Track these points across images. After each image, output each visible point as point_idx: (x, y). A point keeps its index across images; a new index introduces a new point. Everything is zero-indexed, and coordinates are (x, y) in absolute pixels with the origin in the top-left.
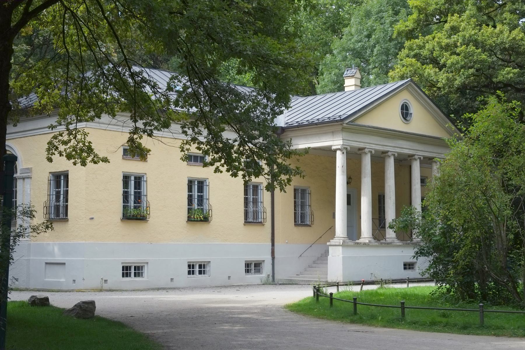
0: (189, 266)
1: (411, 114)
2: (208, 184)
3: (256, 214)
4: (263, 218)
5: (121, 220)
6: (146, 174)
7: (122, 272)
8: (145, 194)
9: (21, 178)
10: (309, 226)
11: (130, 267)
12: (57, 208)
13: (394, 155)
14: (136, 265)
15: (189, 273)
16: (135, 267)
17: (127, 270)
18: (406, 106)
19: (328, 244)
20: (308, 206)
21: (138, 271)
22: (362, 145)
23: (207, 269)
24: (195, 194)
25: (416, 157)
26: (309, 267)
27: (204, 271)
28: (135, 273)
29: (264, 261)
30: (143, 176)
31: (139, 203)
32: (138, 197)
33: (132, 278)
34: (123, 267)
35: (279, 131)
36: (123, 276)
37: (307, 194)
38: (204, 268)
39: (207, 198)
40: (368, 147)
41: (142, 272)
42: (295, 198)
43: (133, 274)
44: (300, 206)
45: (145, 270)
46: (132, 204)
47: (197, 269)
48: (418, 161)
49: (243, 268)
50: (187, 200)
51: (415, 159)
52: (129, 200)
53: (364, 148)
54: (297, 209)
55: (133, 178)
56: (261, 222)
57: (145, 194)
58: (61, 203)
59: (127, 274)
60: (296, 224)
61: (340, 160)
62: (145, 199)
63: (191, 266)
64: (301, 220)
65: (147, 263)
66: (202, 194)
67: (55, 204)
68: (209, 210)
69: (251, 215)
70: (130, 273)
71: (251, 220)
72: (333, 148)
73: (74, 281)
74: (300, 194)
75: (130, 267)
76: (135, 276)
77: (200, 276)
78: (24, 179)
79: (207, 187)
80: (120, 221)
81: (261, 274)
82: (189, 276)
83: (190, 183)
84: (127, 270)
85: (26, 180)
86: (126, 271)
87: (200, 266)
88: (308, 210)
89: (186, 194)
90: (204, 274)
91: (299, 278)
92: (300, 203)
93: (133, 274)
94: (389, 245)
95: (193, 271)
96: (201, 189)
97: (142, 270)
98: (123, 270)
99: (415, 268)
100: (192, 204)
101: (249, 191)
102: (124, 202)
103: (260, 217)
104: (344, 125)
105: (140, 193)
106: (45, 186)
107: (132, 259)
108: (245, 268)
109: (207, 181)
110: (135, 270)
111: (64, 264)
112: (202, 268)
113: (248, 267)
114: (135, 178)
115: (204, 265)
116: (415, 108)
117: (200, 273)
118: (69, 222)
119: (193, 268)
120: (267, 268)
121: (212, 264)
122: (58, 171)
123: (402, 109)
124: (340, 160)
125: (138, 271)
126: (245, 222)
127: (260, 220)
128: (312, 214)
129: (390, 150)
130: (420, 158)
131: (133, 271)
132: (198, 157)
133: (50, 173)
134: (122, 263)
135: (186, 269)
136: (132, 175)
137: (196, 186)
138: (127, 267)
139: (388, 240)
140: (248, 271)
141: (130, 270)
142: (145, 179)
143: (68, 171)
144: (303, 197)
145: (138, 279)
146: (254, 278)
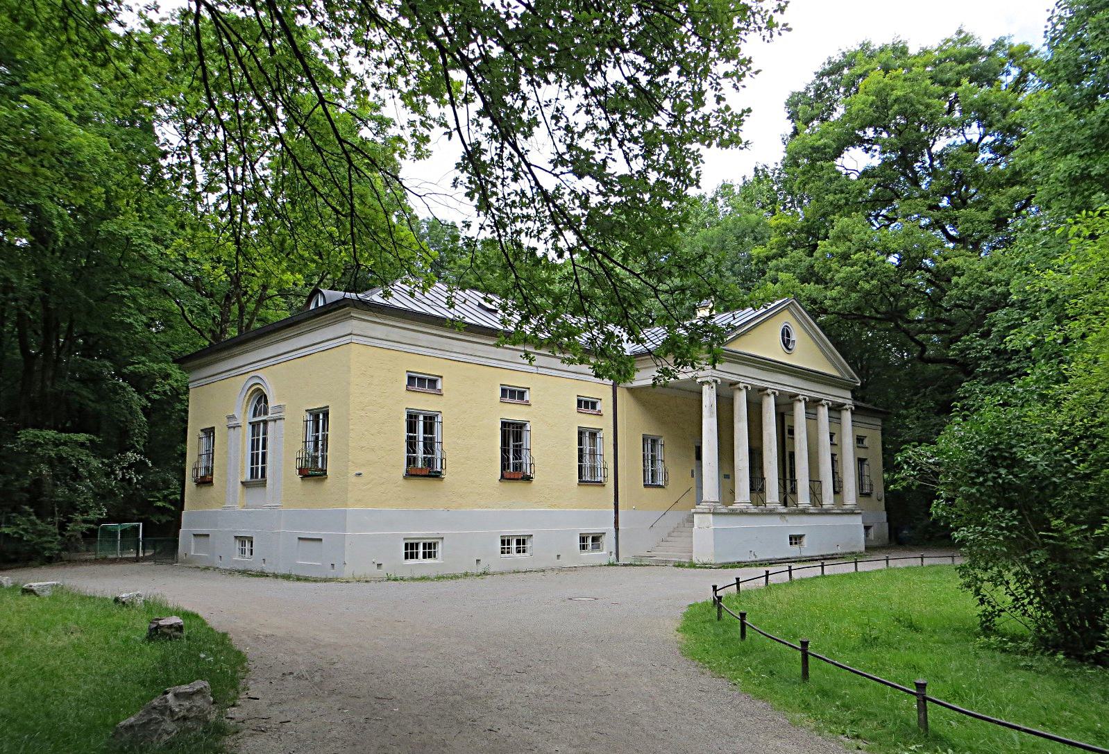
0: (503, 542)
11: (417, 544)
14: (412, 541)
16: (424, 545)
17: (412, 548)
19: (693, 510)
21: (430, 550)
22: (735, 378)
23: (528, 545)
24: (420, 434)
28: (424, 554)
32: (429, 446)
34: (406, 545)
36: (406, 558)
38: (524, 544)
43: (421, 555)
45: (439, 548)
46: (420, 454)
47: (514, 545)
55: (421, 418)
61: (709, 398)
70: (417, 553)
76: (424, 557)
78: (275, 420)
84: (412, 548)
86: (411, 550)
87: (518, 542)
88: (660, 467)
93: (421, 555)
96: (429, 428)
98: (406, 549)
102: (408, 452)
105: (432, 439)
106: (300, 430)
107: (420, 533)
110: (424, 548)
114: (425, 418)
115: (524, 540)
119: (508, 544)
120: (608, 542)
124: (709, 398)
125: (430, 550)
132: (514, 391)
138: (412, 545)
140: (583, 547)
145: (428, 561)
146: (590, 556)
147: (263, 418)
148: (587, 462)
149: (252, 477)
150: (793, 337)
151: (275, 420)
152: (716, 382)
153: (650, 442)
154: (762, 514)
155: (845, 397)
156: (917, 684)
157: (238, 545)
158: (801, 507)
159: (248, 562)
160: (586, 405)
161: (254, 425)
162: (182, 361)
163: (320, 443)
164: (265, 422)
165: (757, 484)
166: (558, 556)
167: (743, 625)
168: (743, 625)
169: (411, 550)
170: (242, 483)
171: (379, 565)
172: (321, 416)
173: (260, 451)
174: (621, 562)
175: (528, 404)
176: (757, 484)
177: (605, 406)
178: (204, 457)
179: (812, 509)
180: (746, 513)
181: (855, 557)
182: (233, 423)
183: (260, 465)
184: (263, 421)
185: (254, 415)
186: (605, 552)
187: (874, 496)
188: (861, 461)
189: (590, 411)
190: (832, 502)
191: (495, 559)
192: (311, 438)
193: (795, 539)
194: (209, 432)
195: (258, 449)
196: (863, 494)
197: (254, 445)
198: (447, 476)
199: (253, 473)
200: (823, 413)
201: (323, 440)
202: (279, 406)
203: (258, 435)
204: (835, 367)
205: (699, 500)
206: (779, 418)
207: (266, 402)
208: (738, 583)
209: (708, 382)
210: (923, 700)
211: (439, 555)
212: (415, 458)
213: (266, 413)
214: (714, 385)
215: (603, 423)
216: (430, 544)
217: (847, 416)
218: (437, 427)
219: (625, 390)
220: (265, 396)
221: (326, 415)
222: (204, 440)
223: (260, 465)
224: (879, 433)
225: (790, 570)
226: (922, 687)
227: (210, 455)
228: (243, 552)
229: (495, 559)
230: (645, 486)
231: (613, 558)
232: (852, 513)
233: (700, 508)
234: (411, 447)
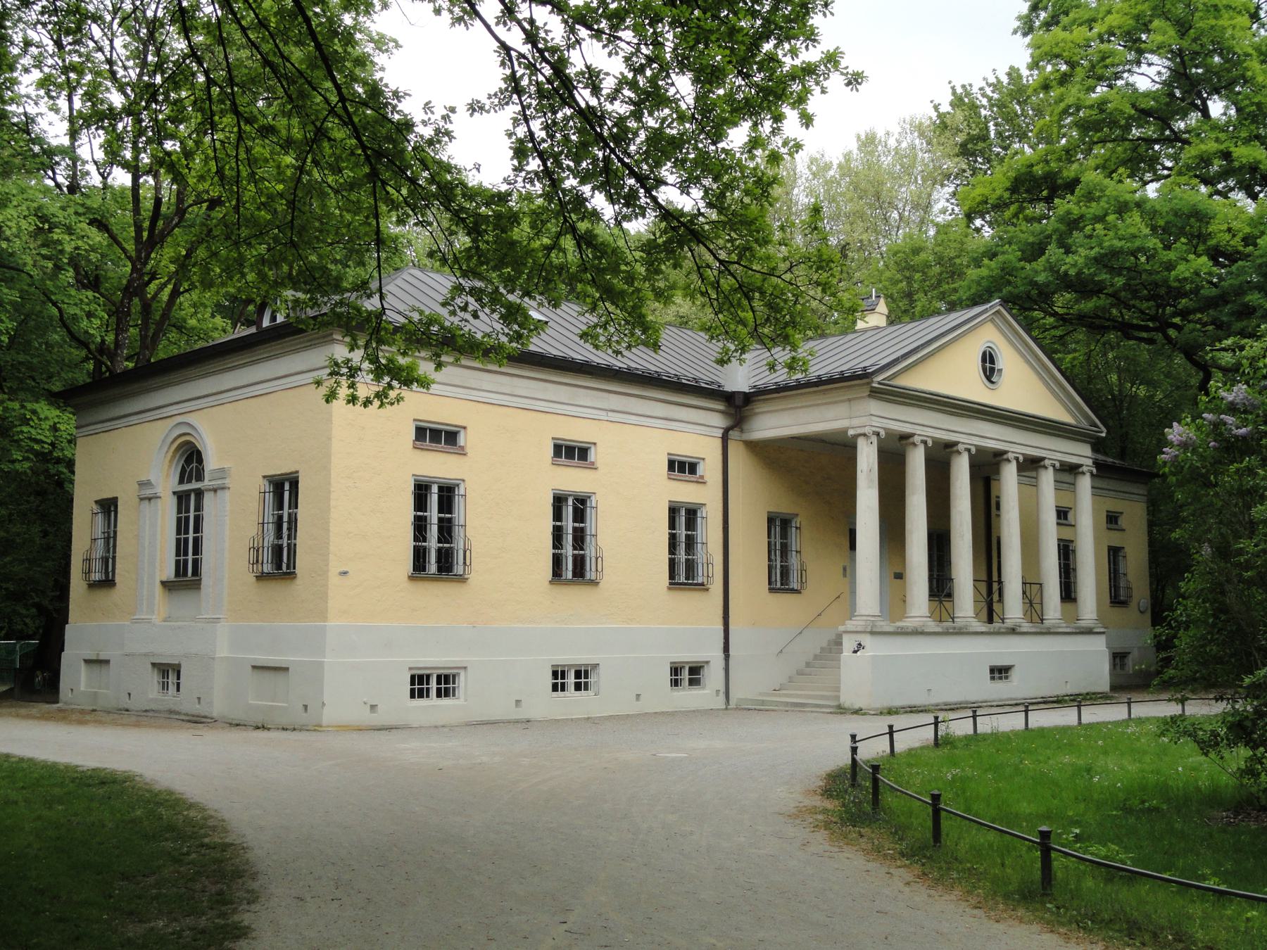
0: (555, 674)
1: (1000, 371)
2: (594, 505)
3: (691, 567)
4: (705, 574)
5: (409, 577)
6: (463, 481)
7: (409, 687)
8: (462, 522)
9: (210, 490)
10: (797, 592)
11: (428, 676)
12: (277, 550)
13: (969, 450)
15: (555, 688)
16: (439, 677)
17: (421, 683)
18: (991, 355)
19: (841, 628)
20: (794, 553)
21: (446, 684)
22: (907, 429)
24: (433, 514)
25: (1010, 456)
26: (800, 673)
27: (586, 684)
28: (439, 690)
29: (707, 662)
30: (458, 485)
31: (582, 549)
33: (433, 701)
34: (413, 677)
35: (739, 401)
36: (412, 696)
37: (794, 529)
38: (586, 677)
39: (593, 533)
40: (918, 432)
41: (454, 689)
42: (769, 536)
43: (433, 692)
44: (778, 553)
45: (461, 681)
47: (571, 680)
48: (1014, 464)
49: (667, 676)
50: (551, 537)
51: (1008, 460)
52: (564, 543)
53: (912, 435)
54: (773, 557)
55: (435, 489)
56: (702, 584)
57: (462, 522)
58: (285, 542)
59: (421, 691)
60: (772, 590)
61: (867, 460)
62: (462, 535)
63: (558, 674)
64: (782, 579)
65: (465, 668)
66: (582, 525)
67: (276, 542)
68: (597, 559)
69: (682, 570)
70: (428, 689)
71: (683, 579)
72: (851, 432)
73: (306, 707)
74: (778, 529)
75: (428, 676)
76: (439, 695)
77: (578, 693)
78: (215, 490)
79: (593, 511)
80: (406, 578)
81: (704, 688)
82: (555, 694)
83: (559, 501)
84: (421, 683)
85: (219, 492)
86: (419, 685)
87: (578, 674)
88: (794, 561)
89: (548, 524)
90: (586, 689)
91: (780, 696)
92: (778, 547)
94: (961, 632)
95: (563, 685)
96: (579, 515)
97: (454, 683)
98: (412, 683)
99: (1010, 679)
100: (451, 537)
101: (677, 519)
103: (700, 573)
104: (874, 385)
107: (433, 659)
108: (669, 678)
109: (593, 498)
110: (439, 682)
111: (287, 669)
112: (583, 677)
113: (676, 674)
114: (441, 489)
115: (586, 672)
116: (1010, 361)
117: (578, 687)
118: (299, 581)
119: (563, 678)
120: (713, 676)
121: (602, 669)
122: (279, 473)
123: (984, 360)
124: (867, 460)
125: (446, 684)
126: (670, 584)
127: (700, 581)
128: (803, 570)
129: (962, 440)
130: (1017, 459)
131: (433, 685)
132: (574, 448)
133: (264, 477)
134: (410, 669)
135: (549, 681)
136: (434, 483)
137: (570, 509)
138: (421, 677)
139: (959, 622)
140: (675, 683)
141: (428, 684)
142: (462, 492)
143: (297, 472)
144: (784, 535)
145: (444, 702)
146: (688, 697)
147: (194, 485)
148: (682, 556)
149: (177, 574)
150: (1000, 364)
151: (215, 490)
152: (878, 434)
153: (779, 525)
154: (946, 633)
155: (1081, 454)
156: (1041, 832)
157: (155, 677)
158: (1009, 623)
159: (170, 699)
160: (682, 467)
161: (182, 498)
162: (69, 398)
163: (285, 526)
164: (199, 494)
165: (941, 586)
166: (638, 696)
167: (937, 812)
168: (937, 812)
169: (419, 685)
170: (163, 583)
171: (373, 707)
172: (287, 487)
173: (191, 535)
174: (733, 704)
175: (592, 467)
176: (941, 586)
177: (710, 469)
178: (101, 543)
179: (1026, 627)
180: (923, 633)
181: (1079, 700)
182: (148, 492)
183: (190, 557)
184: (194, 490)
185: (181, 481)
186: (706, 695)
187: (1133, 604)
188: (1115, 553)
189: (687, 476)
190: (1058, 615)
191: (545, 703)
192: (270, 518)
193: (1000, 672)
194: (108, 507)
195: (187, 532)
196: (1117, 596)
197: (181, 526)
198: (473, 577)
199: (180, 569)
200: (1047, 479)
201: (289, 522)
202: (222, 470)
203: (188, 511)
204: (1069, 410)
205: (852, 611)
206: (981, 485)
207: (200, 461)
208: (891, 732)
209: (864, 435)
210: (1046, 850)
211: (461, 692)
212: (425, 548)
213: (200, 477)
214: (874, 438)
215: (706, 495)
216: (447, 677)
217: (1085, 484)
218: (458, 502)
219: (741, 447)
220: (199, 453)
221: (294, 483)
222: (100, 517)
223: (190, 557)
224: (1144, 506)
225: (936, 723)
226: (1045, 835)
227: (110, 539)
228: (165, 686)
229: (545, 703)
230: (772, 590)
231: (720, 702)
232: (1089, 632)
233: (850, 625)
234: (420, 533)
